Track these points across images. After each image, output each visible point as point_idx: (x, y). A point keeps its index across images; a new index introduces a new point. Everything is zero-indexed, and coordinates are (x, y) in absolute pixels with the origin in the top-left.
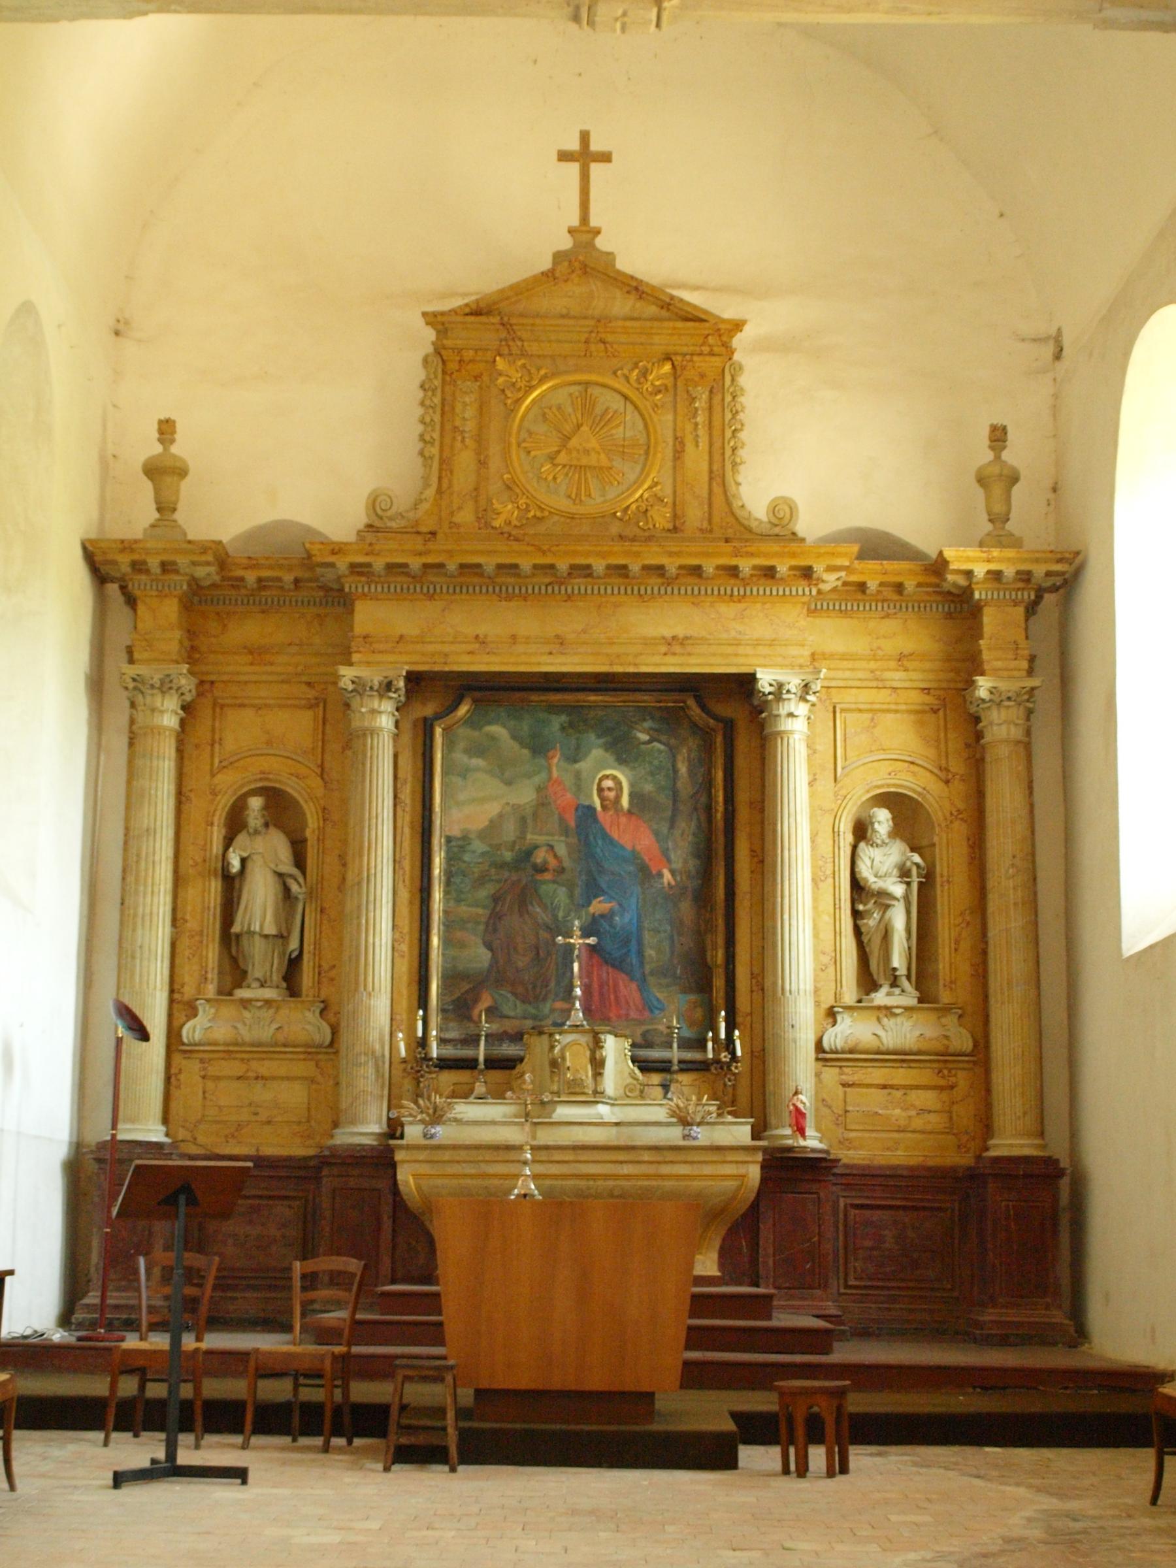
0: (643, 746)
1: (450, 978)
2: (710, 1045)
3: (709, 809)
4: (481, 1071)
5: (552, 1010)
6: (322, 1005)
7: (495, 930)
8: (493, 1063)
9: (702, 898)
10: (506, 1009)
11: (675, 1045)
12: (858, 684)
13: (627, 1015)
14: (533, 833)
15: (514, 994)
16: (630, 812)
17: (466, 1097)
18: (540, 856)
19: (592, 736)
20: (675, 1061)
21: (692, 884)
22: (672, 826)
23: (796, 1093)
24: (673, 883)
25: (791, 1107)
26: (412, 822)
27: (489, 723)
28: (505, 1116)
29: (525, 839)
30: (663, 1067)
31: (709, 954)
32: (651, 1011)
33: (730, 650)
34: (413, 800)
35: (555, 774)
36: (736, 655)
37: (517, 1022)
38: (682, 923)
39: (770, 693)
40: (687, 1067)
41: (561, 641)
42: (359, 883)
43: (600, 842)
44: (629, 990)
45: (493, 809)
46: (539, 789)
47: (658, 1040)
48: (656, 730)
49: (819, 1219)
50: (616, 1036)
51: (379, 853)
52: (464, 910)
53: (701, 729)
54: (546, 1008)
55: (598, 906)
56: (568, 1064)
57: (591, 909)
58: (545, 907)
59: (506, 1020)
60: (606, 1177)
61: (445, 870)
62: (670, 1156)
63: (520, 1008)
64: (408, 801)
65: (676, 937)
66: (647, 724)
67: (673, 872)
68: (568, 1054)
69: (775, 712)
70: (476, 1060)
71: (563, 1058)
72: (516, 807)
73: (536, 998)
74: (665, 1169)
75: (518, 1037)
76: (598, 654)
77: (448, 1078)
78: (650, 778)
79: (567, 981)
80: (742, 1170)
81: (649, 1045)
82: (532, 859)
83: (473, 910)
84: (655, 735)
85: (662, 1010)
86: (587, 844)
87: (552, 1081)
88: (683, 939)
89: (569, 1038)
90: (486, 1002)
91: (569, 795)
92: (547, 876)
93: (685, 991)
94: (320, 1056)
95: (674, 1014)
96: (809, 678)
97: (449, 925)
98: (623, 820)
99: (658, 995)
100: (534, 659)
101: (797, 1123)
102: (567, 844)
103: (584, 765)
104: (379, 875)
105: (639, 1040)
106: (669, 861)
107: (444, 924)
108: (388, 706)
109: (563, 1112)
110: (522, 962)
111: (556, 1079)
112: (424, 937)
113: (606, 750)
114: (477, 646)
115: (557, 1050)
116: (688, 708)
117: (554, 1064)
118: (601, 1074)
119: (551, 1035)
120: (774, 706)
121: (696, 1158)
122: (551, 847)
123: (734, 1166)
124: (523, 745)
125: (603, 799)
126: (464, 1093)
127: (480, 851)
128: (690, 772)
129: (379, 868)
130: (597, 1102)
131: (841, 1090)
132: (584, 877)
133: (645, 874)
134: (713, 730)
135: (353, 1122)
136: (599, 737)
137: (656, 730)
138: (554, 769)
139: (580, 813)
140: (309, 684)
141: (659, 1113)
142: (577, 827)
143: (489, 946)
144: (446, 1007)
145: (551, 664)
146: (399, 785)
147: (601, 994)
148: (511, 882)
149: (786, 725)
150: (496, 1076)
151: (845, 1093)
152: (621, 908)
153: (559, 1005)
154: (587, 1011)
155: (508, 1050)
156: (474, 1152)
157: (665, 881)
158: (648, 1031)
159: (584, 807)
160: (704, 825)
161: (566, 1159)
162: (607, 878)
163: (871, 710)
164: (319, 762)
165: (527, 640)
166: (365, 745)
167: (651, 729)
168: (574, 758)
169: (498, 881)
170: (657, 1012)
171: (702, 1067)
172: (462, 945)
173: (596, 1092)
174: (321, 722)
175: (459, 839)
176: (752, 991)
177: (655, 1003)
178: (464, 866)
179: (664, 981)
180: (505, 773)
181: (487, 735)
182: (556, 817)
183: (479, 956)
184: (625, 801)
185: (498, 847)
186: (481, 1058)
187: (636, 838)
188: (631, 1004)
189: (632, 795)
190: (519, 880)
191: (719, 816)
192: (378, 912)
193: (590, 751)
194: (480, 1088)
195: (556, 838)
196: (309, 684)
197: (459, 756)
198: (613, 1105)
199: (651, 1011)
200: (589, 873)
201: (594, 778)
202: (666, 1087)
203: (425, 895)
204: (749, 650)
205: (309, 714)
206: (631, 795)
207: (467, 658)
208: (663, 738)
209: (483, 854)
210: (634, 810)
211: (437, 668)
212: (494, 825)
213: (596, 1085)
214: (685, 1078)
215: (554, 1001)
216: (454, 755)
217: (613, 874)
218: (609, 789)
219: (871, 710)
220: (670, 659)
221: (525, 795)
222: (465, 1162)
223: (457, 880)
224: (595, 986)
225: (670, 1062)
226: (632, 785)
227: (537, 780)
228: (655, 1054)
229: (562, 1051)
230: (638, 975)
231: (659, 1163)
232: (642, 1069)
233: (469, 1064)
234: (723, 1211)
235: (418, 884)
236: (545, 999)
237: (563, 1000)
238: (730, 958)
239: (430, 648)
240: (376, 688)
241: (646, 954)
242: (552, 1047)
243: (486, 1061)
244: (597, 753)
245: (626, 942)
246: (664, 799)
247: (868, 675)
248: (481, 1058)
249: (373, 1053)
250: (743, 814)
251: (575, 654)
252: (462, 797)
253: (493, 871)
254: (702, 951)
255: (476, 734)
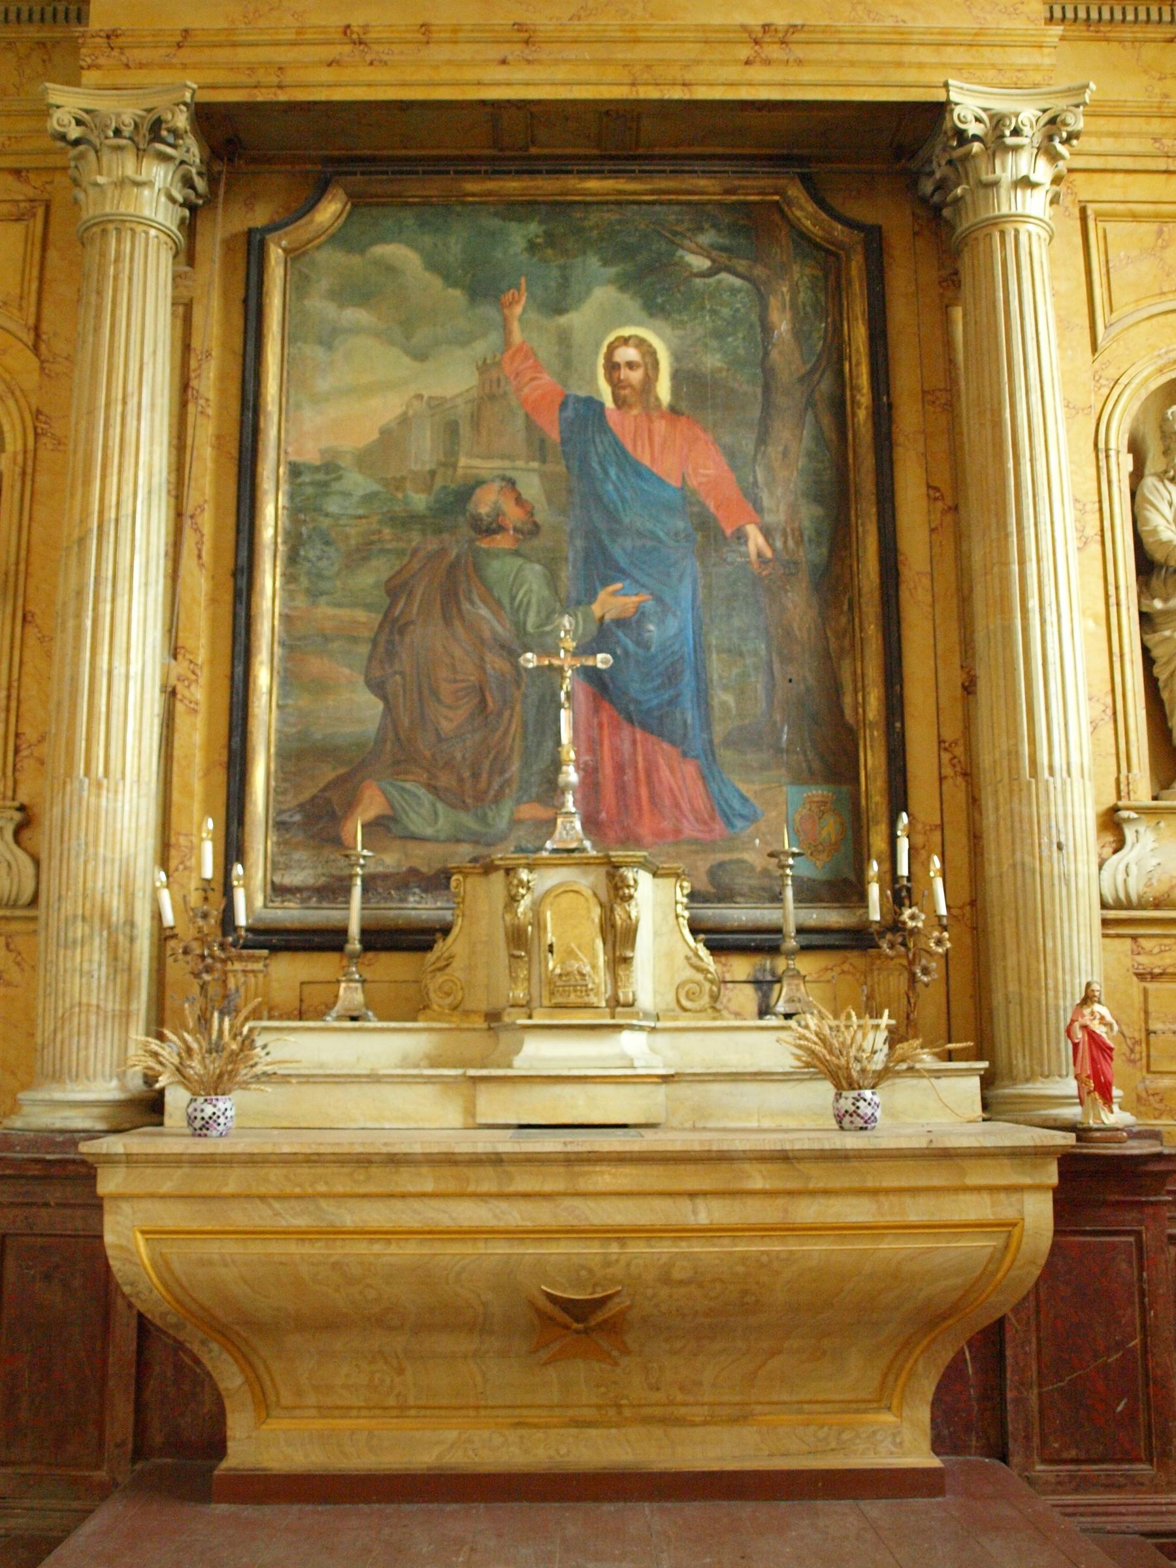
0: (698, 281)
1: (294, 756)
2: (874, 891)
3: (840, 407)
4: (353, 956)
5: (515, 822)
6: (18, 816)
7: (391, 655)
8: (380, 939)
9: (832, 583)
10: (417, 823)
11: (789, 893)
12: (1129, 163)
13: (677, 832)
14: (470, 455)
15: (432, 788)
16: (674, 410)
17: (320, 1015)
18: (485, 502)
19: (594, 262)
20: (791, 929)
21: (811, 555)
22: (762, 440)
23: (1088, 999)
24: (769, 554)
25: (1079, 1035)
26: (219, 437)
27: (382, 240)
28: (405, 1061)
29: (455, 466)
30: (761, 943)
31: (848, 700)
32: (729, 823)
33: (886, 54)
34: (222, 392)
35: (517, 337)
36: (899, 64)
37: (439, 850)
38: (788, 633)
39: (976, 138)
40: (816, 941)
41: (526, 36)
42: (82, 541)
43: (613, 472)
44: (677, 776)
45: (386, 409)
46: (483, 368)
47: (742, 882)
48: (723, 249)
49: (1142, 1294)
50: (655, 875)
51: (128, 474)
52: (325, 611)
53: (818, 247)
54: (501, 818)
55: (611, 602)
56: (550, 937)
57: (597, 609)
58: (496, 606)
59: (411, 845)
60: (650, 1233)
61: (287, 534)
62: (819, 1177)
63: (446, 820)
64: (212, 395)
65: (776, 666)
66: (707, 238)
67: (767, 533)
68: (549, 914)
69: (986, 177)
70: (343, 932)
71: (539, 924)
72: (436, 404)
73: (480, 797)
74: (808, 1211)
75: (438, 882)
76: (605, 62)
77: (288, 972)
78: (714, 344)
79: (546, 758)
80: (1006, 1209)
81: (725, 895)
82: (471, 507)
83: (344, 613)
84: (723, 258)
85: (751, 819)
86: (585, 472)
87: (514, 979)
88: (792, 670)
89: (545, 880)
90: (371, 805)
91: (546, 378)
92: (502, 542)
93: (798, 779)
94: (15, 926)
95: (780, 824)
96: (1058, 104)
97: (294, 644)
98: (660, 426)
99: (743, 788)
100: (469, 74)
101: (1096, 1074)
102: (543, 476)
103: (577, 319)
104: (125, 523)
105: (704, 885)
106: (758, 508)
107: (282, 644)
108: (160, 175)
109: (540, 1052)
110: (450, 718)
111: (523, 974)
112: (239, 670)
113: (623, 288)
114: (347, 49)
115: (523, 906)
116: (789, 203)
117: (517, 938)
118: (627, 961)
119: (509, 871)
120: (983, 165)
121: (889, 1182)
122: (512, 483)
123: (986, 1198)
124: (450, 279)
125: (616, 385)
126: (308, 1009)
127: (361, 492)
128: (798, 334)
129: (126, 509)
130: (619, 1027)
131: (1136, 987)
132: (579, 543)
133: (709, 534)
134: (840, 245)
135: (57, 1077)
136: (606, 263)
137: (723, 249)
138: (516, 326)
139: (569, 413)
140: (17, 172)
141: (770, 1048)
142: (564, 442)
143: (378, 687)
144: (285, 817)
145: (509, 84)
146: (193, 364)
147: (621, 789)
148: (431, 553)
149: (1009, 203)
150: (393, 966)
151: (1145, 992)
152: (666, 609)
153: (530, 811)
154: (591, 824)
155: (420, 908)
156: (304, 1171)
157: (752, 548)
158: (721, 865)
159: (578, 399)
160: (831, 434)
161: (548, 1187)
162: (628, 544)
163: (1157, 217)
164: (31, 321)
165: (455, 34)
166: (103, 254)
167: (712, 246)
168: (557, 304)
169: (400, 553)
170: (739, 823)
171: (858, 939)
172: (321, 687)
173: (615, 1003)
174: (38, 245)
175: (317, 469)
176: (941, 779)
177: (736, 804)
178: (325, 523)
179: (751, 757)
180: (412, 335)
181: (378, 263)
182: (520, 422)
183: (358, 710)
184: (664, 390)
185: (399, 484)
186: (354, 929)
187: (688, 462)
188: (685, 807)
189: (677, 377)
190: (442, 552)
191: (862, 414)
192: (122, 602)
193: (588, 292)
194: (351, 995)
195: (520, 464)
196: (17, 172)
197: (318, 304)
198: (653, 1030)
199: (729, 823)
200: (591, 534)
201: (598, 345)
202: (764, 985)
203: (243, 583)
204: (926, 55)
205: (18, 228)
206: (675, 376)
207: (326, 75)
208: (741, 265)
209: (368, 498)
210: (683, 405)
211: (261, 96)
212: (391, 440)
213: (615, 987)
214: (807, 965)
215: (519, 802)
216: (306, 302)
217: (640, 534)
218: (631, 365)
219: (1157, 217)
220: (758, 73)
221: (454, 379)
222: (278, 1197)
223: (310, 553)
224: (608, 769)
225: (779, 931)
226: (677, 357)
227: (481, 348)
228: (740, 914)
229: (537, 908)
230: (697, 743)
231: (790, 1193)
232: (715, 949)
233: (328, 940)
234: (953, 1310)
235: (228, 562)
236: (498, 799)
237: (539, 800)
238: (895, 707)
239: (244, 55)
240: (127, 131)
241: (715, 702)
242: (513, 899)
243: (364, 932)
244: (603, 295)
245: (671, 677)
246: (746, 385)
247: (1148, 146)
248: (354, 929)
249: (105, 917)
250: (909, 417)
251: (556, 62)
252: (323, 384)
253: (387, 532)
254: (834, 691)
255: (356, 260)
